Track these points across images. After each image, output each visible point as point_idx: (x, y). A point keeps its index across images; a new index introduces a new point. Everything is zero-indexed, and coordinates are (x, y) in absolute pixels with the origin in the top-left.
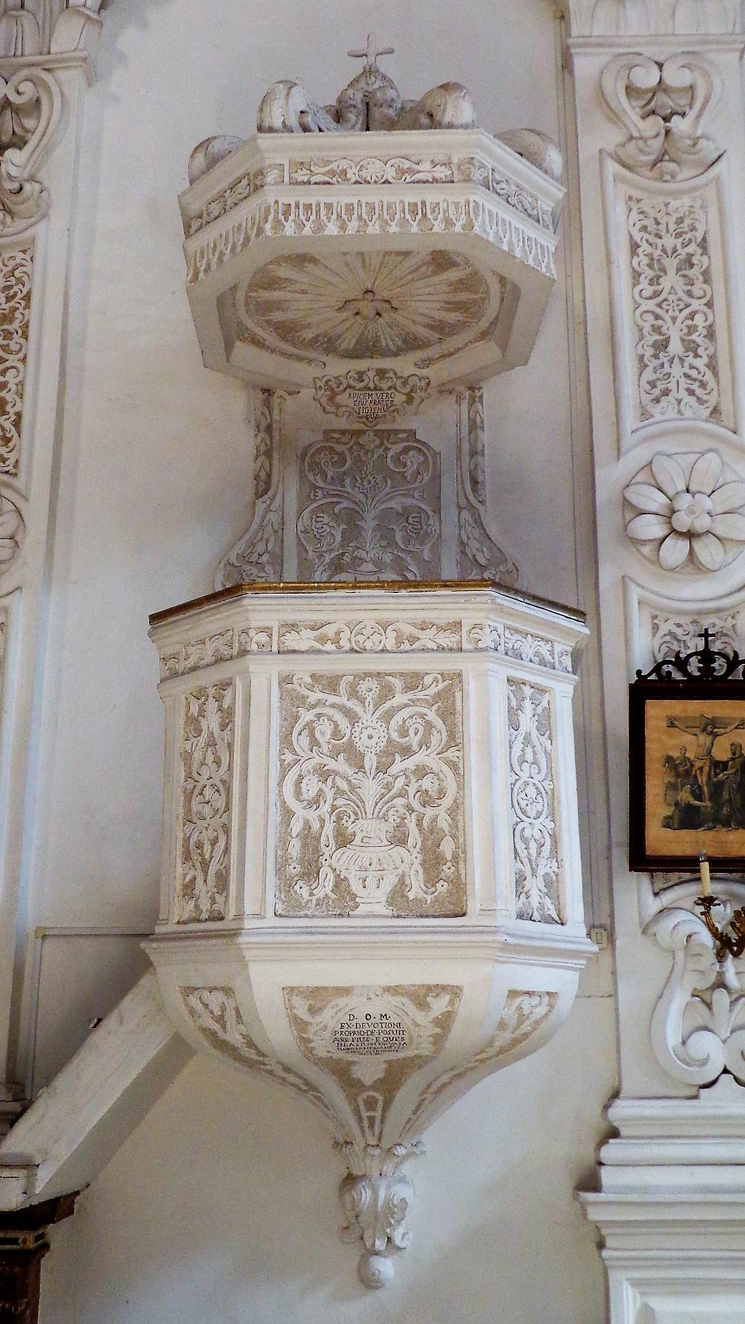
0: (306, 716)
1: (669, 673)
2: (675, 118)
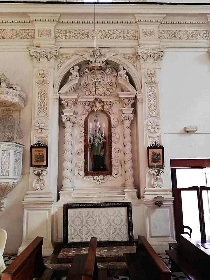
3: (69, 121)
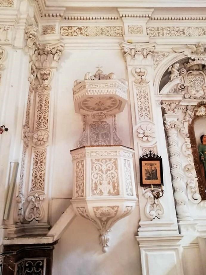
0: (95, 165)
1: (145, 157)
2: (143, 76)
3: (174, 127)
